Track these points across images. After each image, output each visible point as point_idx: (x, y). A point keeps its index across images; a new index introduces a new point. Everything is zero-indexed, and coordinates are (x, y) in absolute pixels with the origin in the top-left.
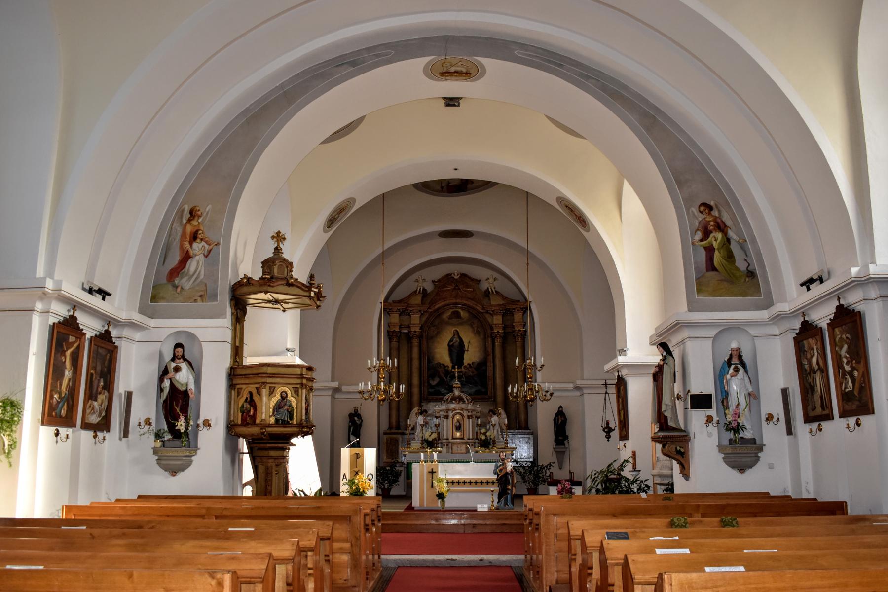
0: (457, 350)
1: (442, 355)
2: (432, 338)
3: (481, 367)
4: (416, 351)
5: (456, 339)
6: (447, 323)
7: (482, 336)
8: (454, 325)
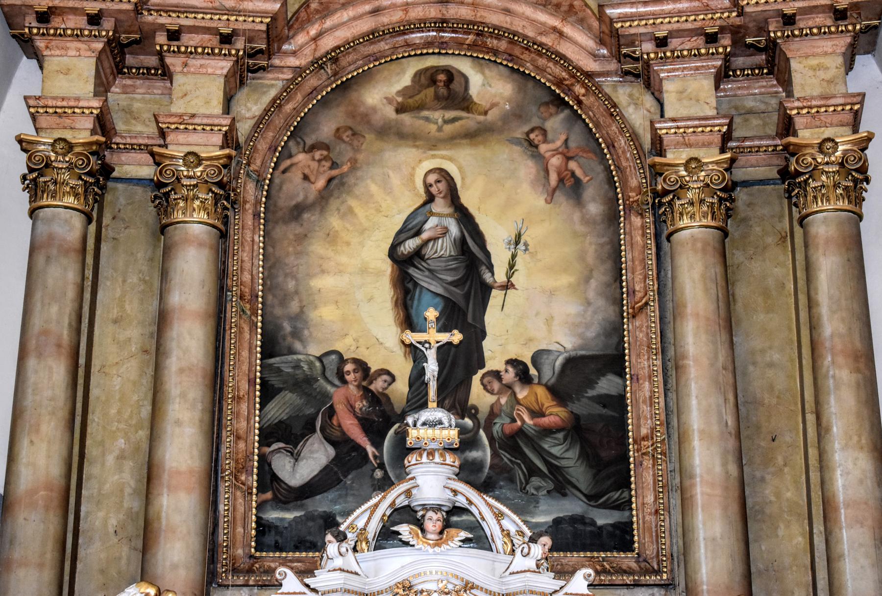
0: (449, 278)
1: (351, 306)
2: (297, 211)
3: (590, 377)
4: (193, 267)
5: (441, 221)
6: (390, 133)
7: (595, 208)
8: (433, 144)
